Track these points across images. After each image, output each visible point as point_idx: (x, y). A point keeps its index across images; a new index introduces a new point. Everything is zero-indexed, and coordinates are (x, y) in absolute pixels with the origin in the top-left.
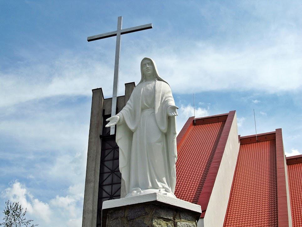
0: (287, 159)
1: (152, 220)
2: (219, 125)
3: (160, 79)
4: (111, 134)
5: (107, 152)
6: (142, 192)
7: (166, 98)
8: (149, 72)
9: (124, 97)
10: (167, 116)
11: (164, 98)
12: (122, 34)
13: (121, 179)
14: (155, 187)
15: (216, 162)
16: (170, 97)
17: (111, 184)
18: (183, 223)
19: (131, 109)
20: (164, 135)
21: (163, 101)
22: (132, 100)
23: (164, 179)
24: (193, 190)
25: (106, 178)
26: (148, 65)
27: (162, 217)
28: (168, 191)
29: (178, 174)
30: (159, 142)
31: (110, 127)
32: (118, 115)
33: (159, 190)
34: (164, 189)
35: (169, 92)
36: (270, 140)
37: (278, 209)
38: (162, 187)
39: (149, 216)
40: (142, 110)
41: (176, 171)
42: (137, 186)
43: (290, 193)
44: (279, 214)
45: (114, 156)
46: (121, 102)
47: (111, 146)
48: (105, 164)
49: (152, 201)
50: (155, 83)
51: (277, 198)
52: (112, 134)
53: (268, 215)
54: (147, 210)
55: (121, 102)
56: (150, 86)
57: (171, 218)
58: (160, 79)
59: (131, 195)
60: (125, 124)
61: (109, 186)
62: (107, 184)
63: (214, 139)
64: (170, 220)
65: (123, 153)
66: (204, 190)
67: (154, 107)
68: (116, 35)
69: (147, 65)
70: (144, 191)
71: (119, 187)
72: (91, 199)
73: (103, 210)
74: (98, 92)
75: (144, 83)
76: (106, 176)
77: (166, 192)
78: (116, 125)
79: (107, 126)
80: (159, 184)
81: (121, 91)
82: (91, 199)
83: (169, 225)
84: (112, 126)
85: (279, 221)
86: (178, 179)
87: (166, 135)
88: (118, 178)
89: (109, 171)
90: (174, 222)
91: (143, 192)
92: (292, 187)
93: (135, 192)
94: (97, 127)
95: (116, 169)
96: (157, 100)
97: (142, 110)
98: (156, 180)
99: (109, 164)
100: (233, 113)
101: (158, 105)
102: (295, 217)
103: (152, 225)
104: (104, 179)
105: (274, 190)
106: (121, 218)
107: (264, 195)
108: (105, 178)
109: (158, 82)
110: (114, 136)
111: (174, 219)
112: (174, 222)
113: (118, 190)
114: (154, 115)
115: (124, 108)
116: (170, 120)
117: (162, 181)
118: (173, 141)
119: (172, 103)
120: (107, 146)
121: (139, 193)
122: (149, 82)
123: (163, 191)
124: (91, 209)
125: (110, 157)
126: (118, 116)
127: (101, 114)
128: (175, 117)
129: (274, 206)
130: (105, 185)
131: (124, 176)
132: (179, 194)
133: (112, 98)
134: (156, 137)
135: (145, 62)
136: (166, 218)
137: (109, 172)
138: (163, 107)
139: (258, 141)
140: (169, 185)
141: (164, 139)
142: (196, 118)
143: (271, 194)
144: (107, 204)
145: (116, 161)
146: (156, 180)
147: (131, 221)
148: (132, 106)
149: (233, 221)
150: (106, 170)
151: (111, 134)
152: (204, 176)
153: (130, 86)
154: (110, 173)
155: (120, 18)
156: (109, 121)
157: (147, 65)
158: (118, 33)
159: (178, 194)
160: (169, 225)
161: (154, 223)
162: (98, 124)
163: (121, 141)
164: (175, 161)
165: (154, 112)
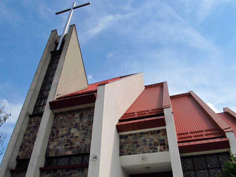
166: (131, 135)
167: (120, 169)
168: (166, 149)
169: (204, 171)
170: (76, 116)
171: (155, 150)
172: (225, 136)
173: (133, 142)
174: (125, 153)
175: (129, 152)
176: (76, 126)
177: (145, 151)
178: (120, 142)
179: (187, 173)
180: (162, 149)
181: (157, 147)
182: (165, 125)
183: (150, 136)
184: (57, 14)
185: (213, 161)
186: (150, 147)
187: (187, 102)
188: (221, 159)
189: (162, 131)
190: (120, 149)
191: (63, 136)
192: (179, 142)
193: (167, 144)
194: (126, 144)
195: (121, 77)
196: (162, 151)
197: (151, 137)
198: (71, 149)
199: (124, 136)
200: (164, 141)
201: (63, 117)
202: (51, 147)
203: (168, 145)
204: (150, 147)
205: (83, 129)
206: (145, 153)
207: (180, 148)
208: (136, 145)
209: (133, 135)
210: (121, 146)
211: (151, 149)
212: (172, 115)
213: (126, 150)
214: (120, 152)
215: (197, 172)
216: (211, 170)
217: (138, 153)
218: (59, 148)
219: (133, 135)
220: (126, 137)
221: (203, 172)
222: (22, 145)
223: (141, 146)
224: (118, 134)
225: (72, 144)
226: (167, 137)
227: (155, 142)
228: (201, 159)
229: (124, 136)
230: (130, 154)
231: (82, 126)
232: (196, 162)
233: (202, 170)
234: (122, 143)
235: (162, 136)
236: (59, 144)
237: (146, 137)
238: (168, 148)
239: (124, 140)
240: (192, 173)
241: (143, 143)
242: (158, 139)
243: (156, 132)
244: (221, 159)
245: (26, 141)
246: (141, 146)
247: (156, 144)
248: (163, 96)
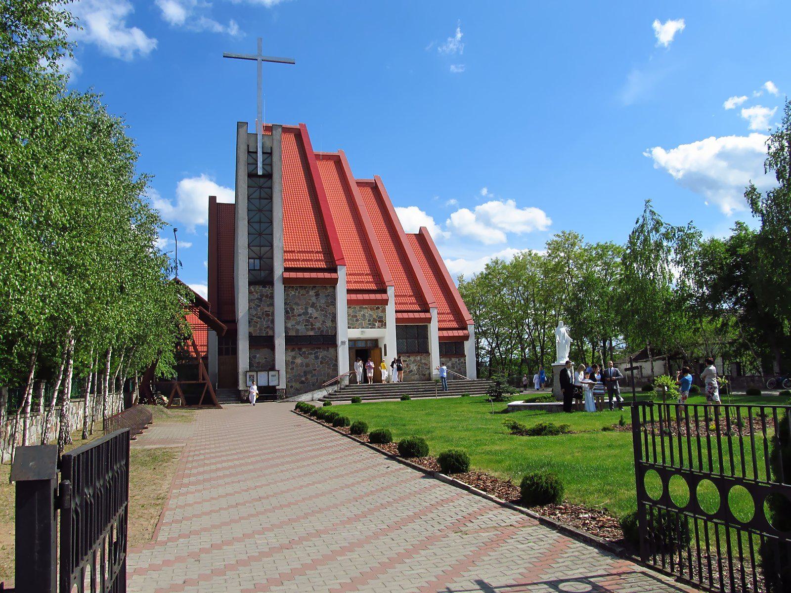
89: (256, 209)
170: (310, 293)
176: (313, 305)
184: (224, 57)
191: (299, 315)
195: (271, 154)
198: (312, 329)
201: (295, 292)
202: (289, 325)
205: (322, 311)
211: (370, 324)
218: (299, 327)
224: (274, 333)
225: (312, 325)
231: (320, 306)
236: (298, 323)
247: (375, 320)
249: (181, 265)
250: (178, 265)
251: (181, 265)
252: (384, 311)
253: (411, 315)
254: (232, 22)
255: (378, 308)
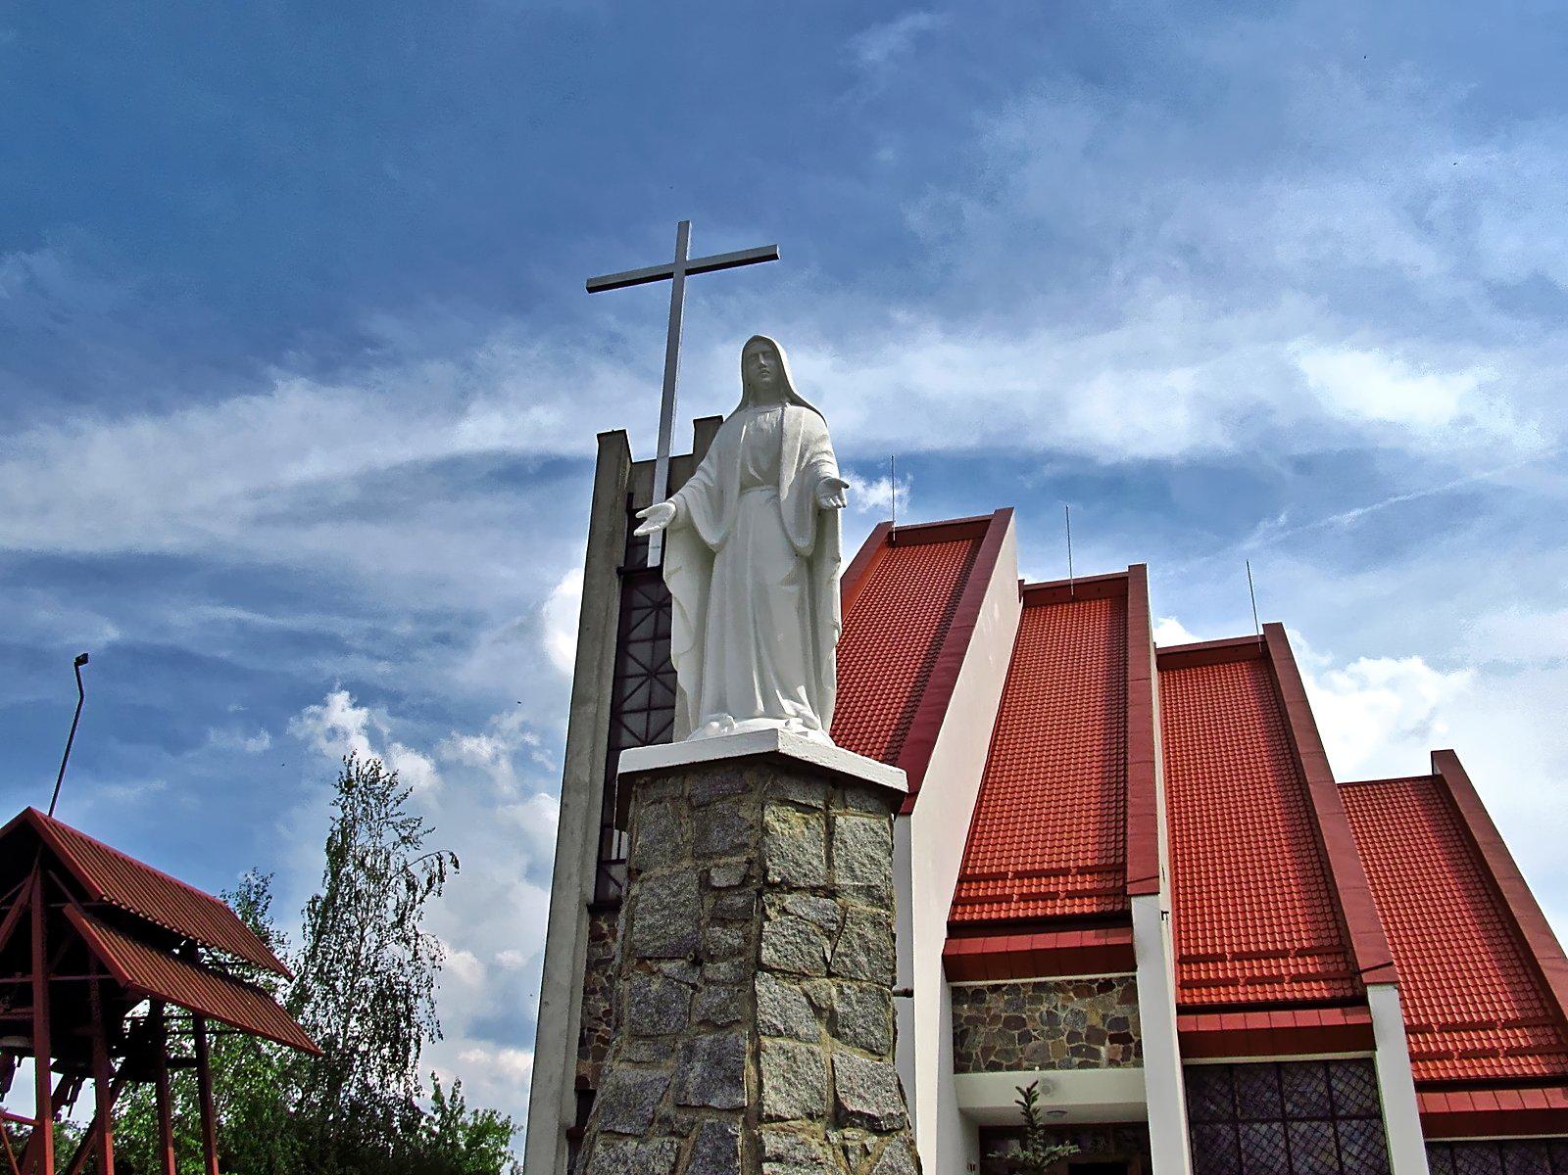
0: (1159, 653)
1: (763, 809)
2: (960, 549)
3: (797, 401)
4: (649, 565)
5: (636, 615)
6: (736, 725)
7: (812, 457)
8: (767, 379)
9: (690, 458)
10: (813, 511)
11: (808, 455)
12: (689, 272)
13: (675, 694)
14: (773, 711)
15: (952, 655)
16: (826, 452)
17: (645, 710)
18: (854, 820)
19: (712, 485)
20: (805, 564)
21: (803, 464)
22: (715, 460)
23: (802, 691)
24: (888, 722)
25: (633, 692)
26: (765, 358)
27: (793, 801)
28: (809, 723)
29: (846, 633)
30: (790, 581)
31: (646, 537)
32: (671, 501)
33: (785, 721)
34: (802, 721)
35: (823, 438)
36: (1110, 597)
37: (1129, 797)
38: (794, 714)
39: (755, 796)
40: (744, 488)
41: (838, 685)
42: (721, 707)
43: (1168, 785)
44: (1130, 811)
45: (656, 629)
46: (680, 470)
47: (649, 599)
48: (631, 653)
49: (764, 753)
50: (783, 410)
51: (1125, 764)
52: (652, 565)
53: (1098, 825)
54: (749, 777)
55: (680, 470)
56: (768, 419)
57: (819, 803)
58: (797, 401)
59: (705, 735)
60: (690, 528)
61: (638, 715)
62: (635, 707)
63: (945, 590)
64: (816, 809)
65: (683, 614)
66: (914, 733)
67: (778, 482)
68: (669, 276)
69: (761, 356)
70: (741, 723)
71: (670, 719)
72: (587, 751)
73: (620, 774)
74: (613, 443)
75: (751, 410)
76: (631, 684)
77: (806, 729)
78: (665, 531)
79: (639, 531)
80: (786, 704)
81: (683, 443)
82: (586, 752)
83: (813, 822)
84: (652, 532)
85: (1129, 831)
86: (840, 686)
87: (812, 562)
88: (667, 691)
89: (643, 671)
90: (827, 816)
91: (740, 727)
92: (1173, 784)
93: (716, 724)
94: (611, 542)
95: (663, 668)
96: (785, 460)
97: (744, 488)
98: (778, 692)
99: (641, 652)
100: (1004, 516)
101: (789, 475)
102: (1178, 845)
103: (762, 823)
104: (628, 694)
105: (1117, 776)
106: (673, 799)
107: (1086, 777)
108: (628, 691)
109: (790, 408)
110: (660, 569)
111: (828, 808)
112: (827, 816)
113: (664, 729)
114: (778, 505)
115: (691, 482)
116: (823, 520)
117: (797, 700)
118: (831, 582)
119: (831, 470)
120: (639, 598)
121: (726, 729)
122: (765, 408)
123: (796, 725)
124: (587, 779)
125: (643, 630)
126: (671, 506)
127: (622, 504)
128: (839, 510)
129: (1116, 827)
130: (631, 712)
131: (685, 680)
132: (839, 731)
133: (655, 460)
134: (781, 568)
135: (754, 349)
136: (803, 802)
137: (642, 675)
138: (803, 482)
139: (1074, 600)
140: (816, 707)
141: (806, 575)
142: (895, 525)
143: (1108, 768)
144: (633, 760)
145: (661, 642)
146: (778, 692)
147: (703, 809)
148: (714, 475)
149: (995, 861)
150: (632, 668)
151: (649, 565)
152: (919, 684)
153: (706, 428)
154: (644, 678)
155: (683, 227)
156: (644, 519)
157: (761, 356)
158: (678, 272)
159: (843, 735)
160: (813, 822)
161: (769, 818)
162: (612, 535)
163: (679, 582)
164: (833, 638)
165: (777, 496)
166: (996, 988)
167: (956, 1113)
168: (1133, 1058)
169: (1270, 1127)
171: (1089, 1060)
172: (1362, 1001)
173: (1006, 1018)
174: (977, 1061)
175: (992, 1058)
177: (1052, 1060)
178: (955, 1017)
179: (1207, 1130)
180: (1119, 1058)
181: (1096, 1047)
182: (1134, 968)
183: (1073, 999)
185: (1310, 1089)
186: (1073, 1045)
187: (1238, 685)
188: (1341, 1087)
189: (1119, 985)
190: (955, 1044)
192: (1182, 1010)
193: (1136, 1039)
194: (979, 1025)
196: (1118, 1065)
197: (1077, 1004)
199: (970, 992)
200: (1128, 1027)
203: (1139, 1044)
204: (1073, 1045)
206: (1052, 1066)
207: (1183, 1037)
208: (1016, 1033)
209: (1004, 989)
210: (959, 1030)
211: (1076, 1052)
212: (1160, 925)
213: (979, 1049)
214: (957, 1055)
215: (1243, 1129)
216: (1295, 1125)
217: (1025, 1064)
219: (1007, 993)
220: (978, 995)
221: (1264, 1128)
222: (586, 1031)
223: (1036, 1039)
226: (1136, 1010)
227: (1091, 1028)
228: (1264, 1081)
229: (970, 992)
230: (995, 1067)
232: (1242, 1090)
233: (1263, 1122)
234: (962, 1021)
235: (1118, 1003)
237: (1059, 1005)
238: (1139, 1054)
239: (969, 1008)
240: (1223, 1132)
241: (1046, 1028)
242: (1104, 1017)
243: (1095, 986)
244: (1341, 1087)
245: (600, 1019)
246: (1036, 1039)
247: (1096, 1036)
248: (1131, 712)
249: (457, 866)
250: (449, 868)
251: (457, 866)
252: (1130, 994)
253: (1509, 1100)
254: (453, 733)
255: (1107, 986)
